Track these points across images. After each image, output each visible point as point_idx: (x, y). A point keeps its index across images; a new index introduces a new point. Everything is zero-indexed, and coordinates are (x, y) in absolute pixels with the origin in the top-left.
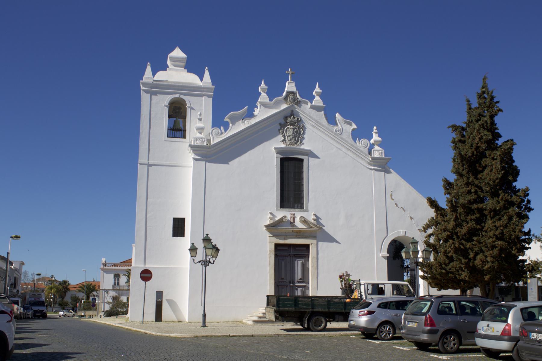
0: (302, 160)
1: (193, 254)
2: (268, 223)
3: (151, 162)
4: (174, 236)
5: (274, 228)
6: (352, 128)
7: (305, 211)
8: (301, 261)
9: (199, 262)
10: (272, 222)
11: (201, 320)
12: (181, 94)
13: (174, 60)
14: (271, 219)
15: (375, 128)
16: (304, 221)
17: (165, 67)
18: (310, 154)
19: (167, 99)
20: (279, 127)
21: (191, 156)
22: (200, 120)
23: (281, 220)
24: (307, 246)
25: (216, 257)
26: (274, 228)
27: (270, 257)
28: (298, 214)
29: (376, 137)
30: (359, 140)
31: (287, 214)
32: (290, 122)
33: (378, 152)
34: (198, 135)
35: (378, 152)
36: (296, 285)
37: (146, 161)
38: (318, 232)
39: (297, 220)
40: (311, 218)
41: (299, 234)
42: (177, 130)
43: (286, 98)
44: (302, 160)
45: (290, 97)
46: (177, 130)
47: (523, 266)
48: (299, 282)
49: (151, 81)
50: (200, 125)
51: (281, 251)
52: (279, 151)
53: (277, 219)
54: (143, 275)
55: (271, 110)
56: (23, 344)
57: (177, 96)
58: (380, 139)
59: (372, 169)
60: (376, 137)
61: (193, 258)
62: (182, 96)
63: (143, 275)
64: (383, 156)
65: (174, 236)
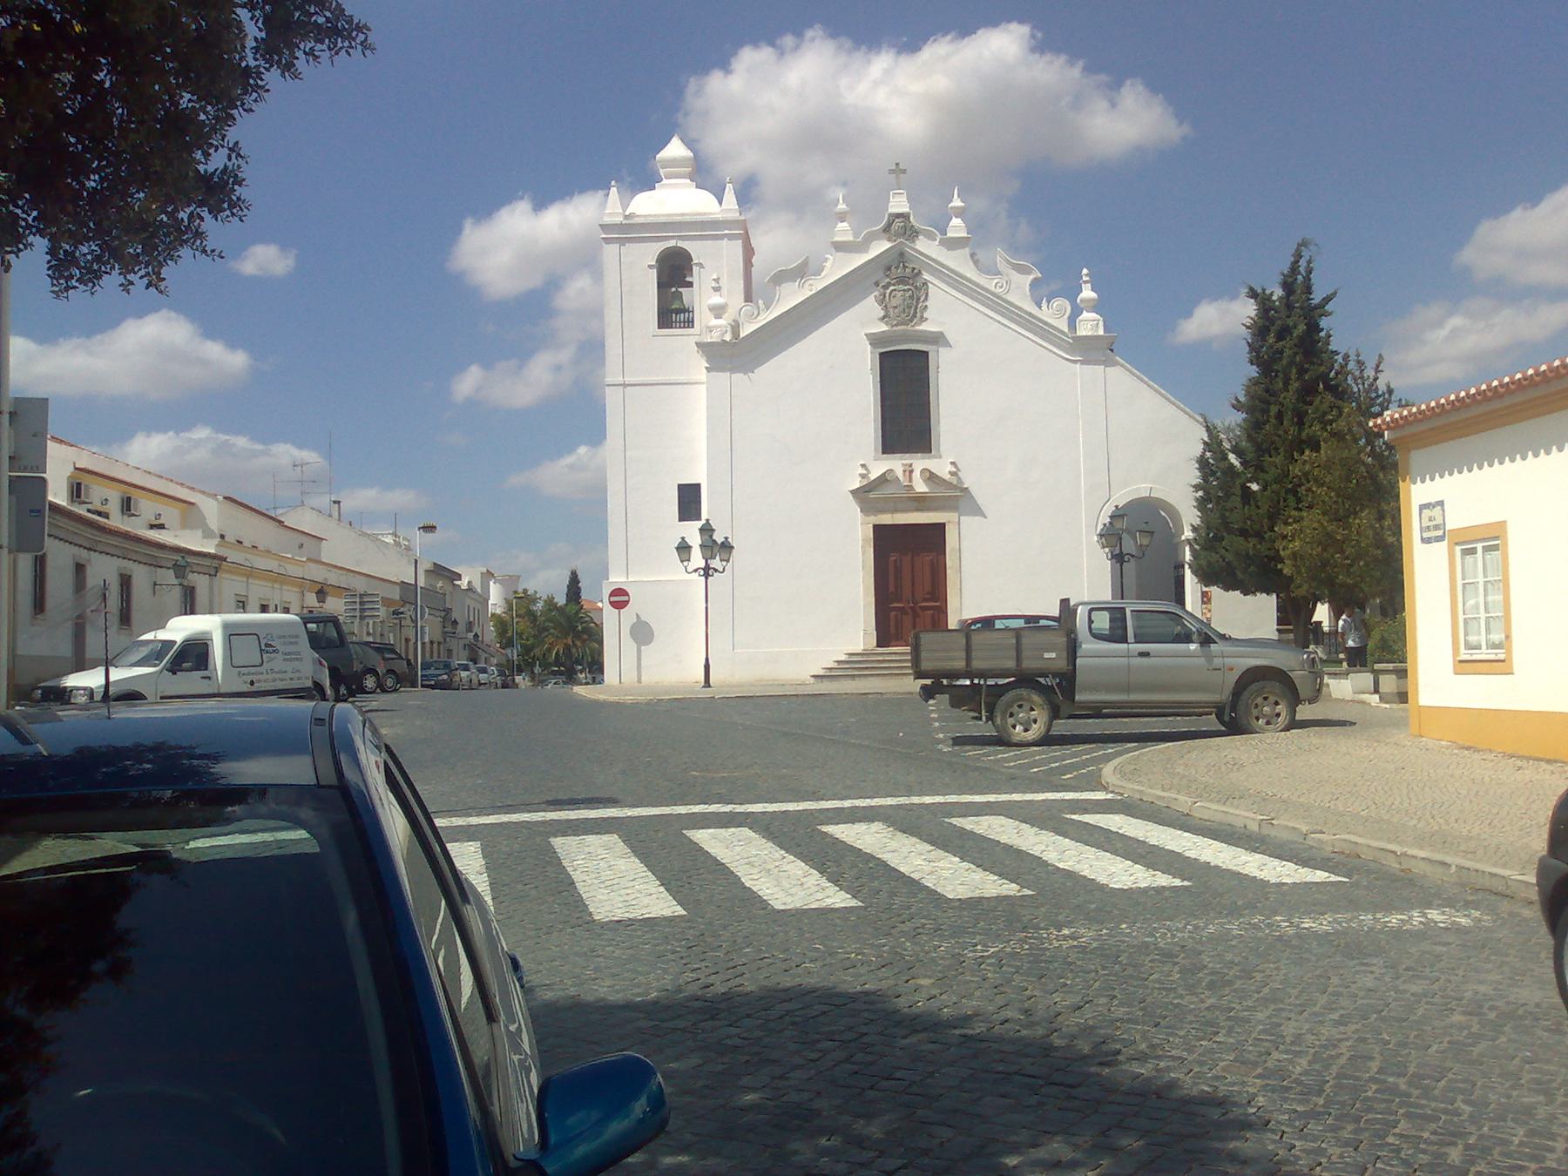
1: (685, 556)
3: (628, 380)
4: (681, 520)
5: (867, 495)
6: (1031, 277)
11: (702, 678)
12: (680, 238)
13: (673, 163)
14: (863, 476)
15: (1085, 271)
16: (931, 477)
17: (648, 181)
18: (938, 339)
19: (657, 248)
21: (698, 367)
22: (717, 289)
23: (883, 480)
24: (941, 527)
26: (867, 495)
27: (864, 553)
28: (920, 463)
29: (1087, 293)
31: (895, 464)
33: (1090, 324)
34: (714, 322)
35: (1090, 324)
37: (620, 380)
38: (954, 495)
39: (916, 474)
40: (942, 469)
41: (921, 502)
42: (672, 314)
43: (887, 229)
45: (898, 224)
46: (672, 314)
47: (561, 610)
48: (925, 600)
49: (619, 219)
50: (716, 300)
51: (883, 536)
52: (875, 340)
53: (873, 477)
55: (857, 255)
56: (1009, 849)
57: (672, 243)
58: (1093, 295)
59: (1075, 362)
60: (1087, 293)
64: (1101, 332)
65: (681, 520)
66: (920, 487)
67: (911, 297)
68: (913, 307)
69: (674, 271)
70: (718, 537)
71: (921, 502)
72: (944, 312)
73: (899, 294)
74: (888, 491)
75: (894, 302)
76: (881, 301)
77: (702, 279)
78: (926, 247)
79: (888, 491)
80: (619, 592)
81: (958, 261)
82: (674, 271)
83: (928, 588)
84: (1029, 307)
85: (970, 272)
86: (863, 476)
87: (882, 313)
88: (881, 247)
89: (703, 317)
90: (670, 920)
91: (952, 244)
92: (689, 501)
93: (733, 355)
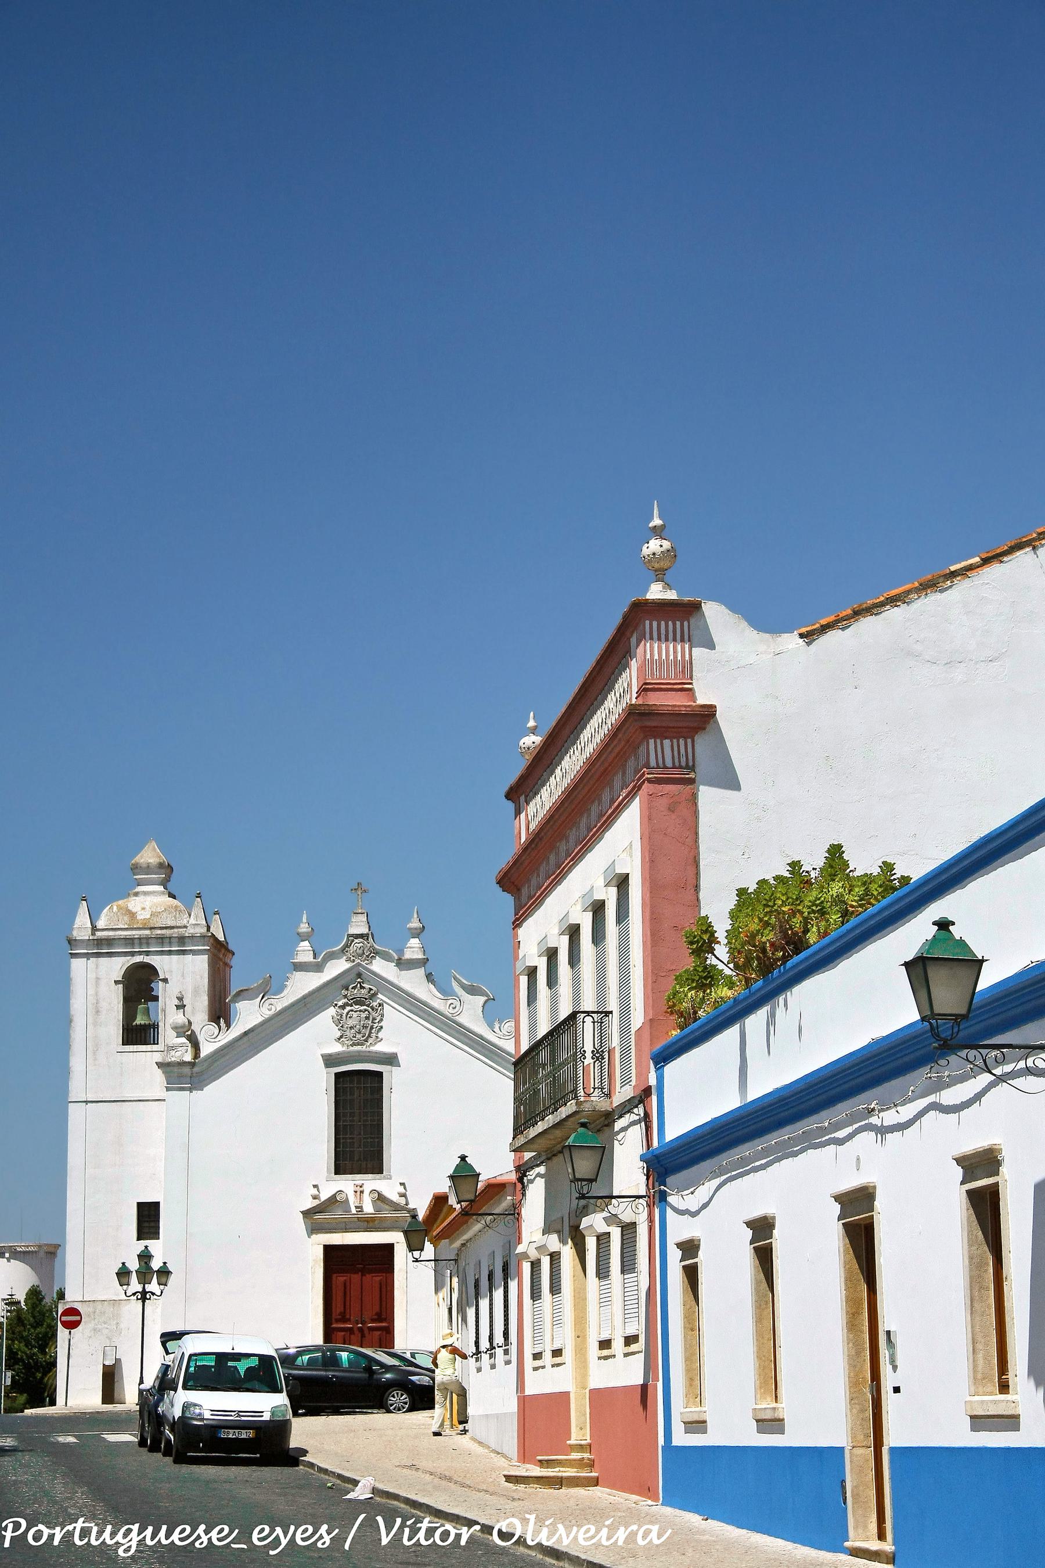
0: (380, 1074)
1: (125, 1280)
2: (310, 1204)
4: (157, 1204)
7: (385, 1178)
8: (379, 1278)
9: (134, 1294)
10: (316, 1202)
16: (380, 1198)
18: (391, 1060)
20: (510, 806)
23: (333, 1200)
25: (166, 1285)
26: (318, 1217)
28: (371, 1183)
30: (500, 1023)
31: (347, 1185)
32: (357, 994)
36: (334, 1326)
40: (390, 1190)
42: (137, 1034)
44: (380, 1074)
51: (336, 1259)
52: (330, 1061)
54: (78, 1318)
57: (138, 959)
61: (125, 1287)
62: (147, 959)
63: (78, 1318)
66: (368, 1208)
67: (367, 1018)
68: (370, 1029)
69: (140, 986)
70: (156, 1264)
71: (369, 1224)
72: (398, 1033)
73: (356, 1017)
74: (338, 1214)
75: (351, 1022)
76: (338, 1021)
77: (166, 994)
78: (379, 966)
79: (338, 1214)
80: (72, 1311)
81: (413, 982)
82: (140, 986)
83: (377, 1309)
84: (480, 1028)
85: (654, 1098)
86: (315, 1197)
87: (339, 1034)
88: (338, 967)
89: (168, 1036)
90: (648, 819)
91: (403, 964)
92: (148, 1219)
93: (190, 1075)
